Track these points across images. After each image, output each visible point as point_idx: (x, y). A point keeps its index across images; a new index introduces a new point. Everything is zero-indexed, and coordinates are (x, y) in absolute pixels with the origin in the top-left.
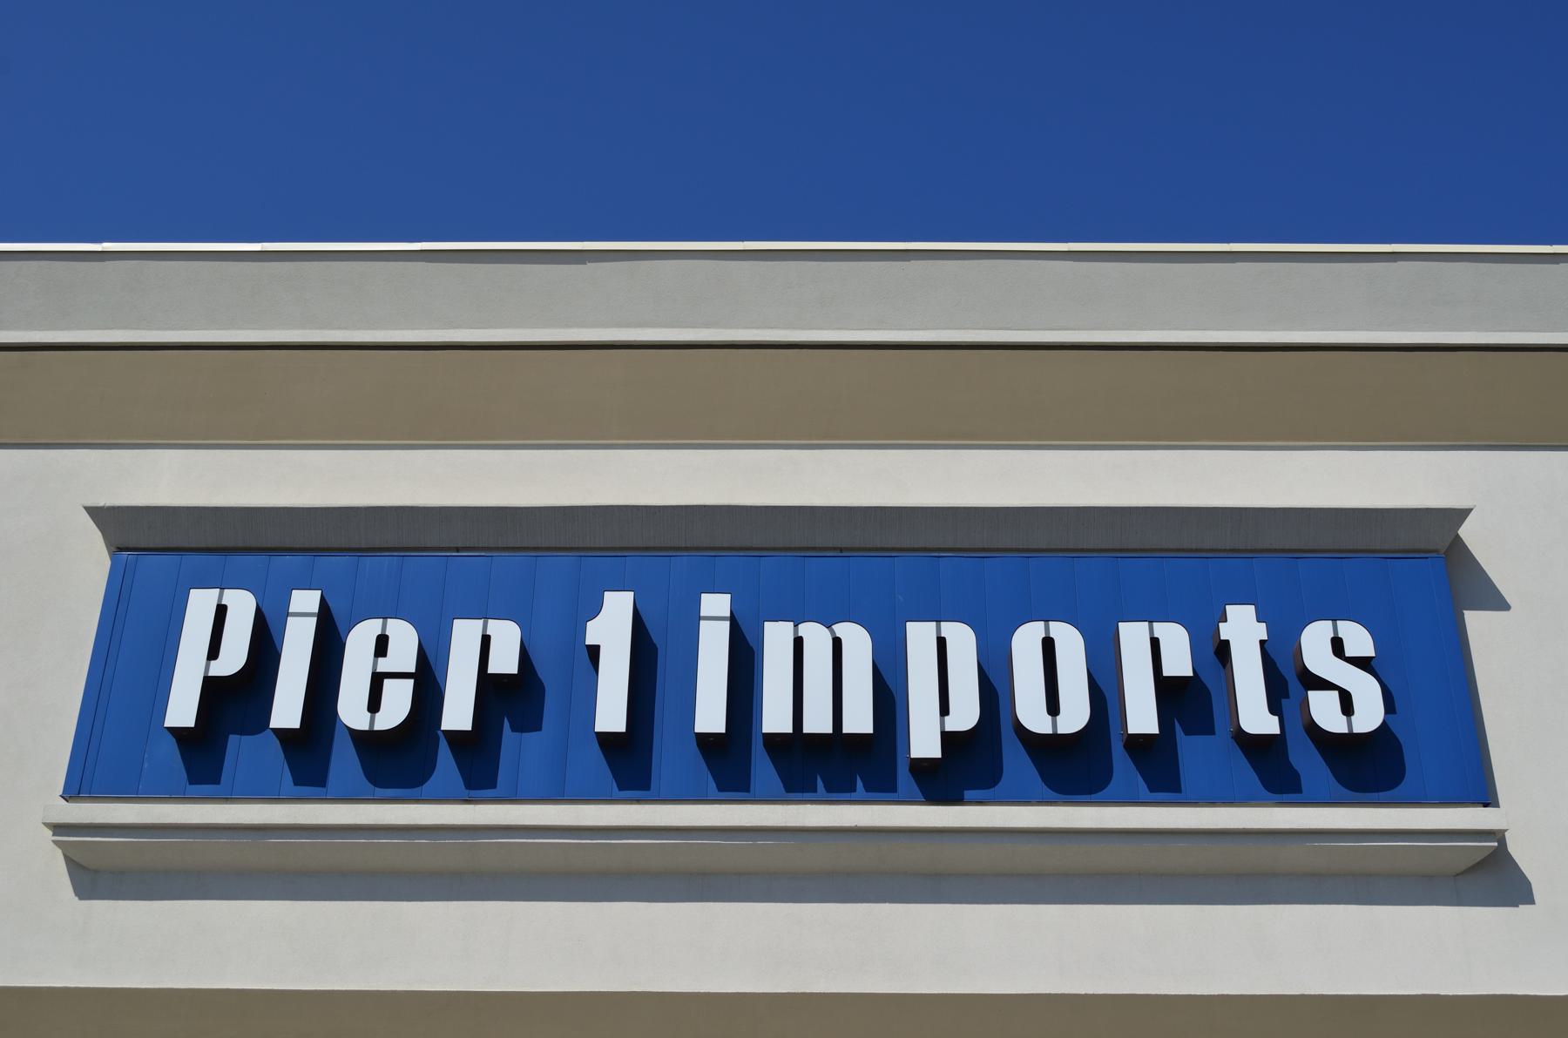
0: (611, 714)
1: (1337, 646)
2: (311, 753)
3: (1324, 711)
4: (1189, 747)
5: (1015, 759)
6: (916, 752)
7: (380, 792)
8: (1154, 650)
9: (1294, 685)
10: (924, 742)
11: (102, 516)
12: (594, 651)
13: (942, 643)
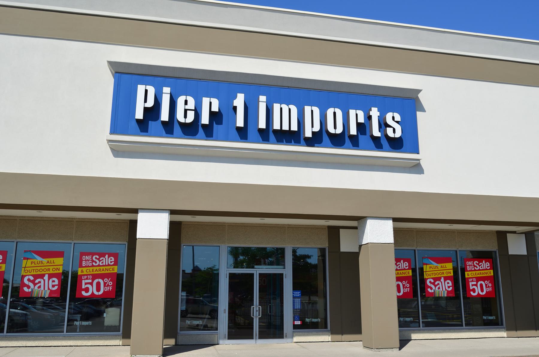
0: (240, 123)
1: (393, 118)
2: (169, 127)
3: (390, 132)
4: (361, 138)
5: (325, 138)
6: (306, 136)
7: (186, 137)
8: (356, 116)
9: (383, 126)
10: (308, 134)
11: (112, 64)
12: (235, 108)
13: (281, 109)
